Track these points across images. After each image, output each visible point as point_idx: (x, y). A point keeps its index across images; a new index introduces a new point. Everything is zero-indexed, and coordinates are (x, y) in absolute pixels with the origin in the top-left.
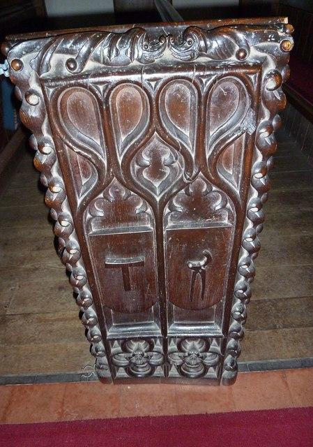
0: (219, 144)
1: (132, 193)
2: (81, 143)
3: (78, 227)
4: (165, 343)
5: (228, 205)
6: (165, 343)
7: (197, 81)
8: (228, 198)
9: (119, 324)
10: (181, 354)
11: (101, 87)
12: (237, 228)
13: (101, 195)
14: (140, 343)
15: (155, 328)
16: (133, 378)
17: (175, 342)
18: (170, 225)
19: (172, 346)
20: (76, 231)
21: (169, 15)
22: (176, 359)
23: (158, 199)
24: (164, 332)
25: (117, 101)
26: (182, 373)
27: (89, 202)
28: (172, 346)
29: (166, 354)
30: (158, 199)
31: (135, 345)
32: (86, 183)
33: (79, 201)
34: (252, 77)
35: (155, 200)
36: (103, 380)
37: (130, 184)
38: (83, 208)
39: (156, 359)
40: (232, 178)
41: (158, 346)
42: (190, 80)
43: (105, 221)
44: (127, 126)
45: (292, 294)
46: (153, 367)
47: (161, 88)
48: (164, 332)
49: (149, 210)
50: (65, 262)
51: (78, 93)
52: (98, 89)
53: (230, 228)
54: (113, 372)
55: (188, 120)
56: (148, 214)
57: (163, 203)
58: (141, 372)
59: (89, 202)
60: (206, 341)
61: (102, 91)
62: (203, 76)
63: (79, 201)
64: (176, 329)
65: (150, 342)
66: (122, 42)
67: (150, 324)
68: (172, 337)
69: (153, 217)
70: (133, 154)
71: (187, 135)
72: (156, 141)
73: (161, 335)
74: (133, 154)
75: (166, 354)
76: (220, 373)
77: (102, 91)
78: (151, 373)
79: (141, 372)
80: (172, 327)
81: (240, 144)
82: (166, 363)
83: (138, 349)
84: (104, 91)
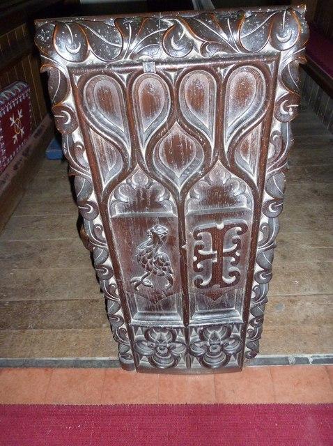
0: (240, 131)
1: (154, 181)
2: (254, 116)
3: (102, 209)
4: (187, 335)
5: (247, 191)
10: (150, 343)
11: (173, 74)
13: (125, 181)
14: (163, 333)
15: (176, 320)
16: (154, 368)
18: (189, 211)
19: (194, 336)
20: (101, 215)
22: (146, 350)
23: (179, 189)
24: (186, 321)
25: (140, 89)
27: (113, 185)
28: (194, 336)
30: (179, 189)
31: (156, 336)
32: (110, 172)
33: (104, 186)
34: (269, 65)
36: (125, 367)
40: (248, 164)
41: (181, 336)
45: (312, 292)
46: (177, 359)
49: (171, 199)
50: (87, 241)
52: (170, 77)
55: (207, 112)
56: (92, 203)
57: (187, 188)
58: (216, 363)
61: (125, 79)
63: (104, 186)
64: (198, 319)
65: (173, 333)
66: (58, 43)
67: (175, 314)
68: (193, 327)
69: (175, 206)
71: (206, 122)
72: (177, 130)
73: (183, 326)
77: (123, 75)
78: (174, 365)
82: (190, 352)
83: (161, 340)
84: (128, 79)
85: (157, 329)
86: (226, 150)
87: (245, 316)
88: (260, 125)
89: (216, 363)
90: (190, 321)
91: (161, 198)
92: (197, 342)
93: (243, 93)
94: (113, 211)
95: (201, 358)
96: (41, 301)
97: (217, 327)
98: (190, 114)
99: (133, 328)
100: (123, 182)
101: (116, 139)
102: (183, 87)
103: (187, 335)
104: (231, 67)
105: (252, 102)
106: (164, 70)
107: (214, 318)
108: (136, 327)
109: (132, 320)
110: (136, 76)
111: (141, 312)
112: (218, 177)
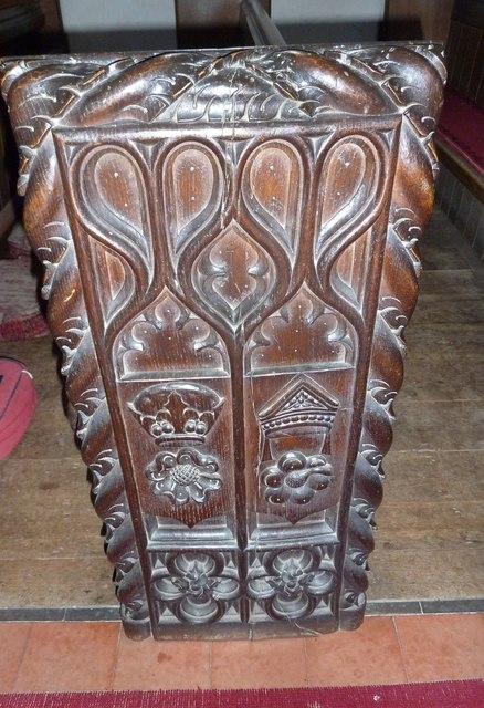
1: (193, 316)
4: (242, 560)
6: (242, 560)
7: (300, 140)
8: (219, 336)
9: (170, 526)
12: (358, 371)
17: (261, 561)
19: (256, 568)
21: (389, 201)
22: (262, 589)
24: (242, 542)
26: (179, 616)
27: (124, 320)
28: (256, 568)
29: (243, 580)
35: (358, 316)
37: (188, 303)
38: (113, 331)
39: (224, 591)
40: (350, 291)
42: (126, 146)
43: (141, 361)
44: (188, 209)
46: (221, 606)
47: (247, 155)
48: (242, 542)
49: (221, 344)
51: (111, 156)
53: (348, 371)
54: (154, 615)
59: (124, 320)
60: (312, 554)
62: (228, 138)
70: (194, 253)
74: (194, 253)
75: (243, 580)
76: (335, 608)
79: (293, 610)
80: (256, 534)
81: (365, 243)
82: (244, 600)
85: (284, 552)
86: (316, 263)
87: (341, 534)
88: (370, 230)
89: (198, 614)
90: (249, 541)
91: (332, 336)
92: (166, 576)
93: (346, 183)
94: (121, 371)
95: (268, 605)
96: (457, 446)
97: (296, 551)
98: (260, 209)
99: (150, 554)
100: (138, 319)
101: (137, 255)
102: (169, 173)
103: (243, 570)
104: (252, 141)
105: (359, 190)
106: (138, 141)
107: (286, 536)
108: (154, 552)
109: (149, 542)
110: (168, 150)
111: (265, 526)
112: (299, 312)
